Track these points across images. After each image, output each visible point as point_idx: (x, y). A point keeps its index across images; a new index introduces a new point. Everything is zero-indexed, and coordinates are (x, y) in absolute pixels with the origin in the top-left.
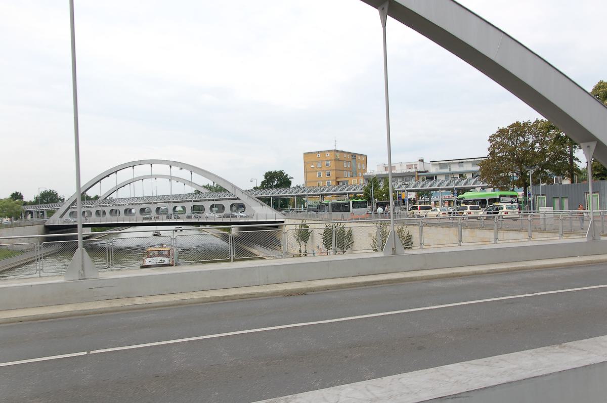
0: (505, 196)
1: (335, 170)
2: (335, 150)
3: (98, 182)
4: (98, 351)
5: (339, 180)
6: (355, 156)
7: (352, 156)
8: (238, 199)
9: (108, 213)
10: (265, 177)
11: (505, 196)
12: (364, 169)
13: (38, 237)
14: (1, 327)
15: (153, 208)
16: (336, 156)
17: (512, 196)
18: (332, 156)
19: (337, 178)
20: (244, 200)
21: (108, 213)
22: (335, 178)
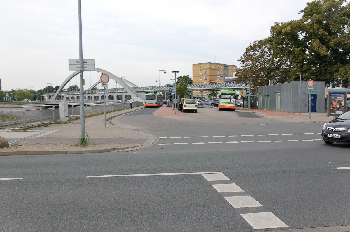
0: (225, 94)
1: (210, 75)
2: (210, 63)
3: (75, 76)
4: (268, 141)
5: (212, 81)
6: (227, 67)
7: (225, 66)
8: (127, 92)
9: (93, 98)
10: (46, 88)
11: (225, 94)
12: (127, 83)
13: (43, 106)
14: (2, 117)
15: (115, 95)
16: (210, 66)
17: (231, 94)
18: (208, 66)
19: (211, 80)
20: (130, 93)
21: (70, 98)
22: (209, 81)
